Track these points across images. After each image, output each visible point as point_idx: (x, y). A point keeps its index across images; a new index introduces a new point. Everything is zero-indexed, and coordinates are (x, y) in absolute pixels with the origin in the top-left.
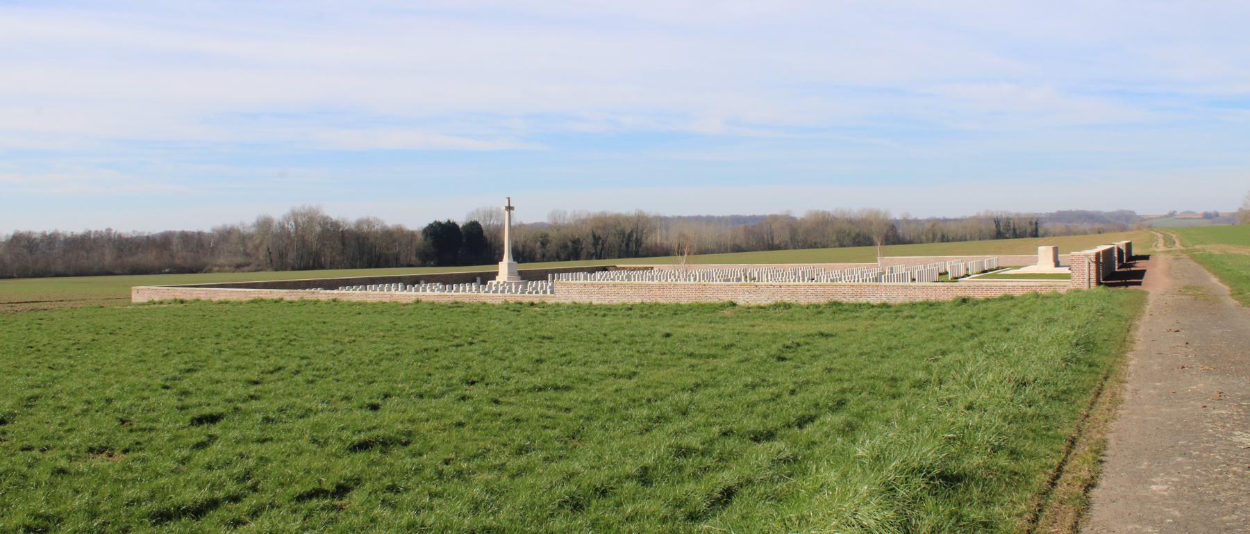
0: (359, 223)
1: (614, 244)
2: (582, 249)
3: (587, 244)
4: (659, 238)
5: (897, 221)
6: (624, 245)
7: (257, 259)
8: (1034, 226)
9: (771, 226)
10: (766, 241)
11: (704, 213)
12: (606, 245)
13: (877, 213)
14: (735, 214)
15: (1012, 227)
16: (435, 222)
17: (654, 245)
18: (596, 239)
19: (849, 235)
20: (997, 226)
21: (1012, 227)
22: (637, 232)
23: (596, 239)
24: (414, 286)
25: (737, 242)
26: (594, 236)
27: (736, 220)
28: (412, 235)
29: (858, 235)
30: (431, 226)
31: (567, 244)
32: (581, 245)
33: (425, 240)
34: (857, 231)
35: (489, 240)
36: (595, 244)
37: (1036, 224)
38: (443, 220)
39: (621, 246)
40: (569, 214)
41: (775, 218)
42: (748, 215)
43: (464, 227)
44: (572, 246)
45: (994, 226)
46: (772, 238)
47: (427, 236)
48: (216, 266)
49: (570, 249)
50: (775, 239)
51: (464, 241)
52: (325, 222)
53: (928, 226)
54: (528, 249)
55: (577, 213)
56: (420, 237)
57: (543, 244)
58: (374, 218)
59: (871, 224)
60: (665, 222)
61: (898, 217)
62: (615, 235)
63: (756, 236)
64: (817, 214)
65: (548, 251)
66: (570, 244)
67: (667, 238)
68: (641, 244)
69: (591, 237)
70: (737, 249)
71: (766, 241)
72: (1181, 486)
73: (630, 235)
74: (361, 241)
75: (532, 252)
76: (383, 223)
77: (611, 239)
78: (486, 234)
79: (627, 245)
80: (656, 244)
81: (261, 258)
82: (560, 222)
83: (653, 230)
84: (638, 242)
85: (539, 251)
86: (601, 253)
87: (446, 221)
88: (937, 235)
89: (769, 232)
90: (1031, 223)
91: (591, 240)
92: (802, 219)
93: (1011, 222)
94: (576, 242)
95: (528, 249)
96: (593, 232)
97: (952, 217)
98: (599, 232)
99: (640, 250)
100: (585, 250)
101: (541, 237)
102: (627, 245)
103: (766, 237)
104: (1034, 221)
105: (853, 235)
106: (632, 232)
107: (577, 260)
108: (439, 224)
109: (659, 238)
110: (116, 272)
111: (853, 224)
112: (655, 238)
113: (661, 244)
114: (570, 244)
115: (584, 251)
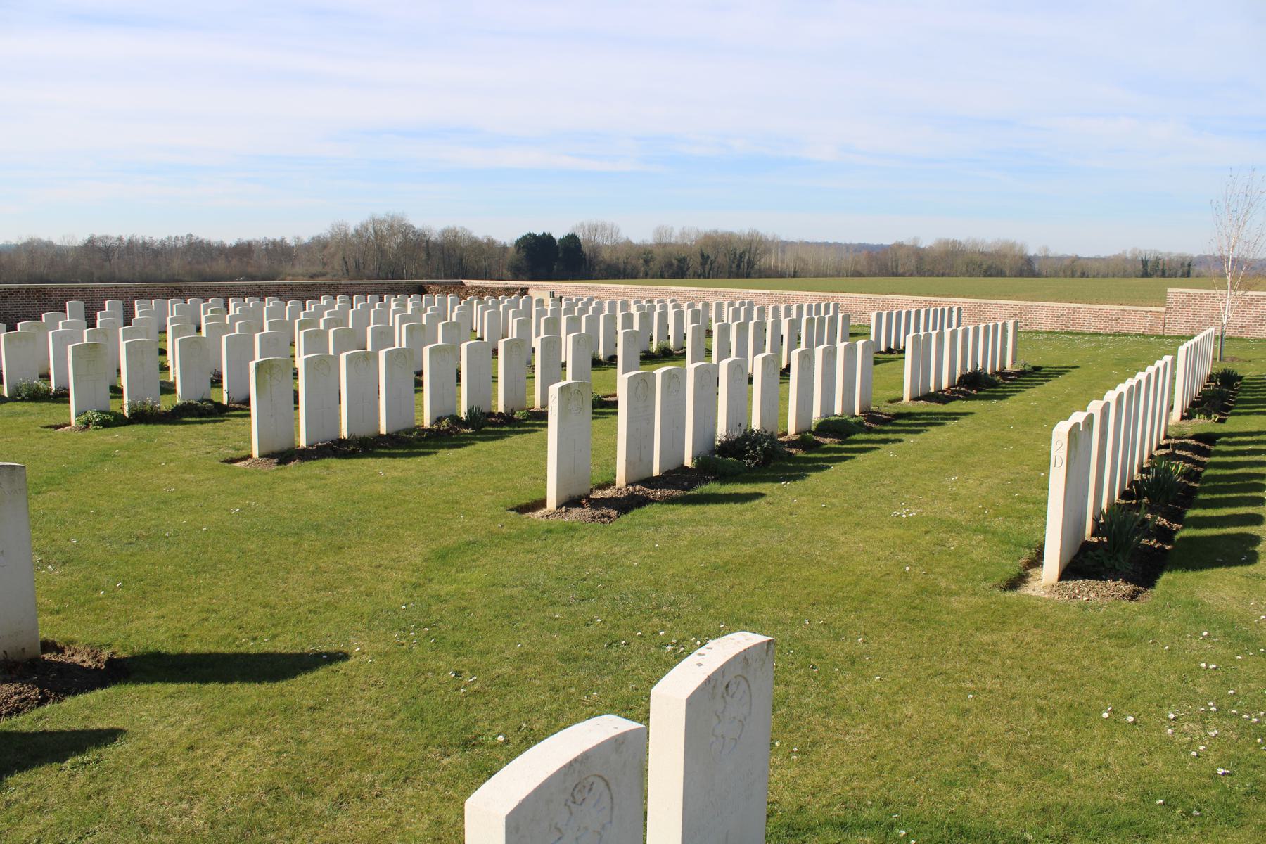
0: (445, 233)
1: (585, 255)
2: (688, 269)
3: (694, 263)
4: (773, 261)
5: (1031, 257)
6: (734, 266)
7: (333, 268)
8: (1186, 268)
9: (896, 254)
10: (890, 269)
11: (831, 240)
12: (715, 265)
13: (1012, 246)
14: (862, 242)
15: (1161, 268)
16: (530, 234)
17: (767, 266)
18: (704, 258)
19: (980, 266)
20: (1144, 266)
21: (1161, 268)
22: (749, 252)
23: (704, 258)
24: (410, 297)
25: (859, 268)
26: (702, 255)
27: (837, 246)
28: (505, 248)
29: (990, 267)
30: (524, 237)
31: (671, 262)
32: (688, 264)
33: (518, 252)
34: (989, 263)
35: (588, 254)
36: (703, 264)
37: (1189, 265)
38: (539, 233)
39: (731, 267)
40: (1128, 253)
41: (900, 246)
42: (875, 244)
43: (560, 240)
44: (678, 266)
45: (1141, 266)
46: (897, 266)
47: (519, 248)
48: (289, 275)
49: (675, 268)
50: (900, 267)
51: (560, 255)
52: (406, 230)
53: (1066, 263)
54: (629, 267)
55: (1137, 253)
56: (513, 250)
57: (646, 262)
58: (461, 228)
59: (1005, 256)
60: (784, 246)
61: (1032, 255)
62: (725, 254)
63: (879, 262)
64: (947, 243)
65: (651, 269)
66: (675, 262)
67: (782, 262)
68: (753, 266)
69: (699, 255)
70: (858, 274)
71: (890, 269)
72: (308, 644)
73: (742, 256)
74: (446, 252)
75: (635, 268)
76: (470, 233)
77: (721, 259)
78: (585, 248)
79: (738, 266)
80: (770, 267)
81: (337, 267)
82: (665, 239)
83: (767, 251)
84: (751, 264)
85: (643, 269)
86: (709, 274)
87: (541, 233)
88: (1076, 271)
89: (894, 259)
90: (1183, 265)
91: (699, 259)
92: (931, 247)
93: (1161, 262)
94: (682, 260)
95: (629, 267)
96: (701, 250)
97: (1085, 256)
98: (707, 251)
99: (752, 272)
100: (691, 270)
101: (645, 254)
102: (738, 266)
103: (890, 264)
104: (1186, 263)
105: (984, 267)
106: (744, 252)
107: (683, 278)
108: (534, 236)
109: (773, 261)
110: (186, 279)
111: (986, 255)
112: (765, 262)
113: (776, 267)
114: (675, 262)
115: (691, 271)
